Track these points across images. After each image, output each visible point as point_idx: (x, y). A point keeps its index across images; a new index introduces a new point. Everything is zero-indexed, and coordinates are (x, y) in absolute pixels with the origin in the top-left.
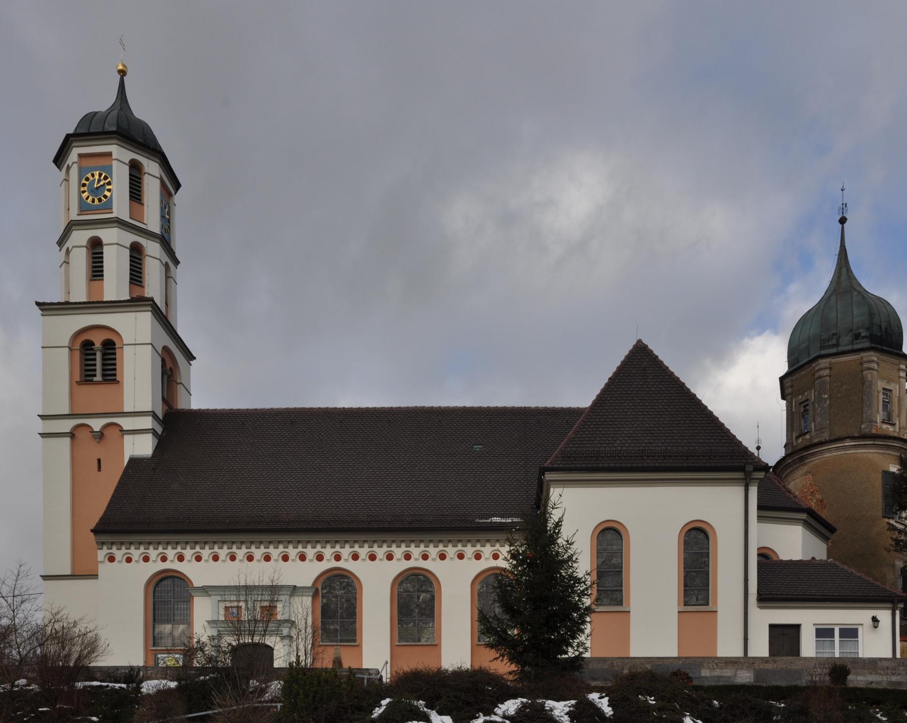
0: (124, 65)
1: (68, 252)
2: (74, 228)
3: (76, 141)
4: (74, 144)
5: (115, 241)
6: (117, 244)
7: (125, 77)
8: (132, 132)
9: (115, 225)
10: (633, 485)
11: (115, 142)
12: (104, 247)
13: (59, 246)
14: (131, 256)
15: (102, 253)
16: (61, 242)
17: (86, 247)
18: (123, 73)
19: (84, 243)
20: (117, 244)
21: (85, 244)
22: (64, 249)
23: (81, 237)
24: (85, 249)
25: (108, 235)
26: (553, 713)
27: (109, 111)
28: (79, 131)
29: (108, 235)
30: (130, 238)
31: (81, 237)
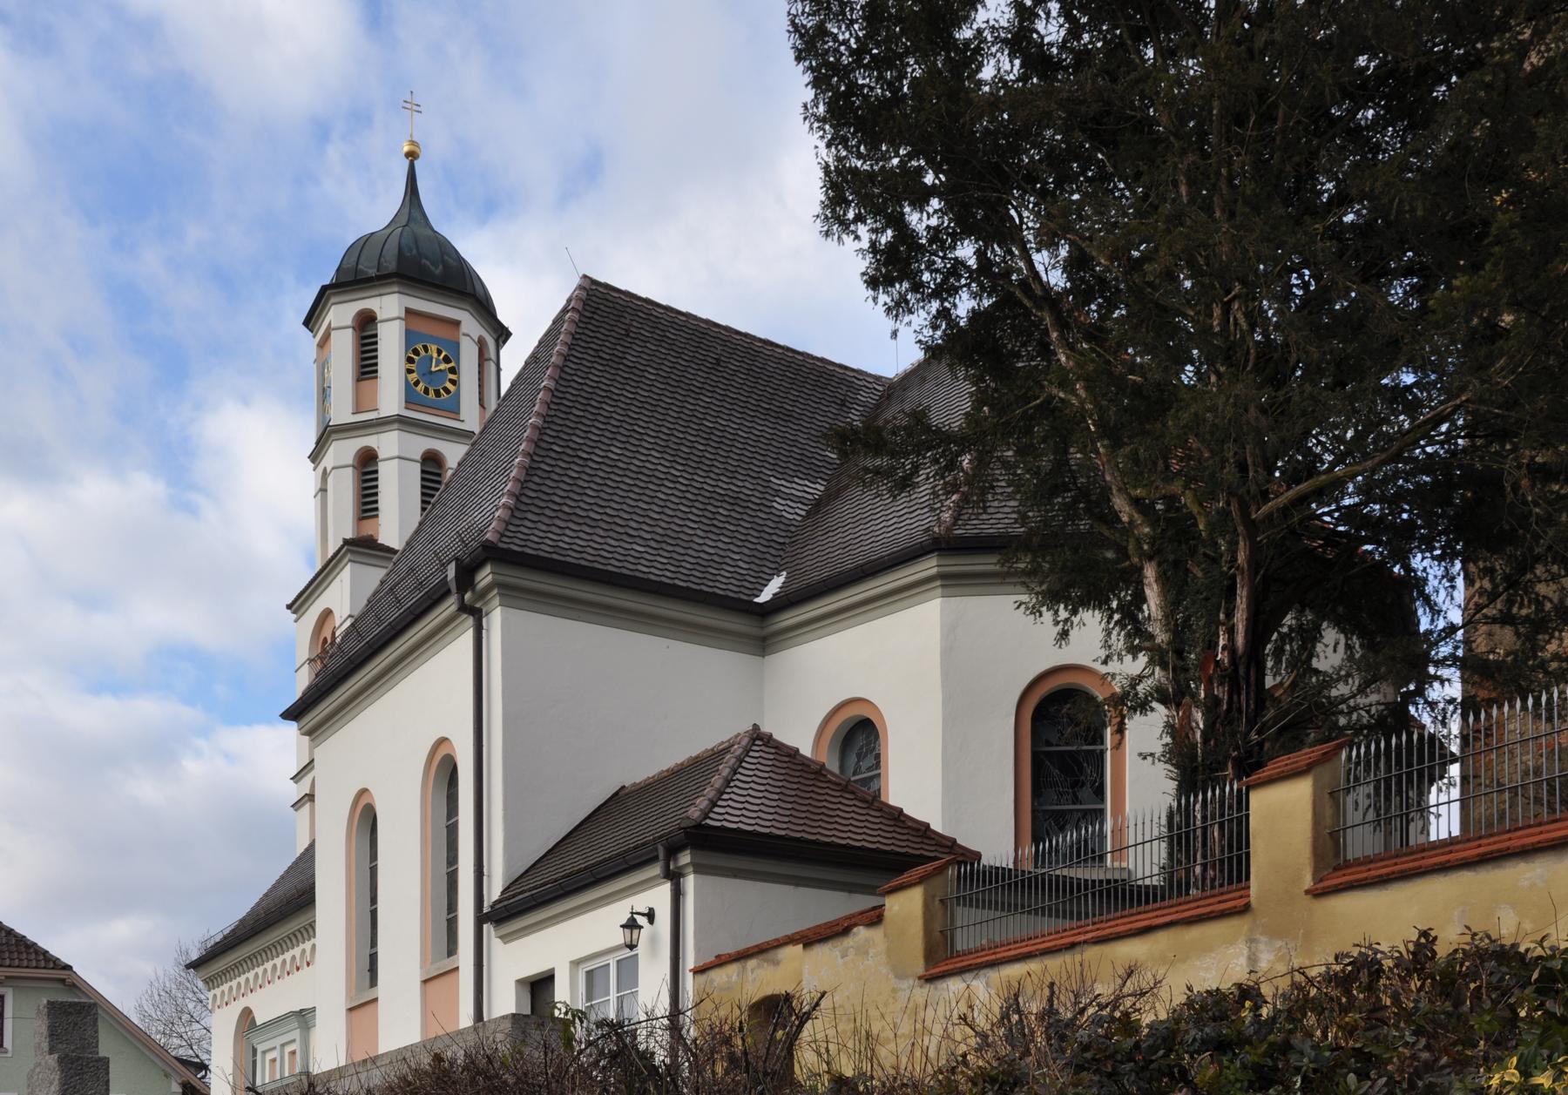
0: (413, 143)
1: (325, 474)
2: (334, 436)
3: (334, 294)
4: (333, 300)
5: (396, 454)
6: (399, 457)
7: (415, 162)
8: (424, 261)
9: (396, 426)
10: (905, 603)
11: (396, 289)
12: (379, 325)
13: (313, 461)
14: (423, 472)
15: (376, 472)
16: (310, 321)
17: (353, 466)
18: (412, 156)
19: (349, 322)
20: (399, 457)
21: (351, 462)
22: (320, 469)
23: (341, 314)
24: (351, 330)
25: (387, 444)
26: (883, 298)
27: (389, 231)
28: (343, 279)
29: (387, 444)
30: (421, 444)
31: (341, 314)
